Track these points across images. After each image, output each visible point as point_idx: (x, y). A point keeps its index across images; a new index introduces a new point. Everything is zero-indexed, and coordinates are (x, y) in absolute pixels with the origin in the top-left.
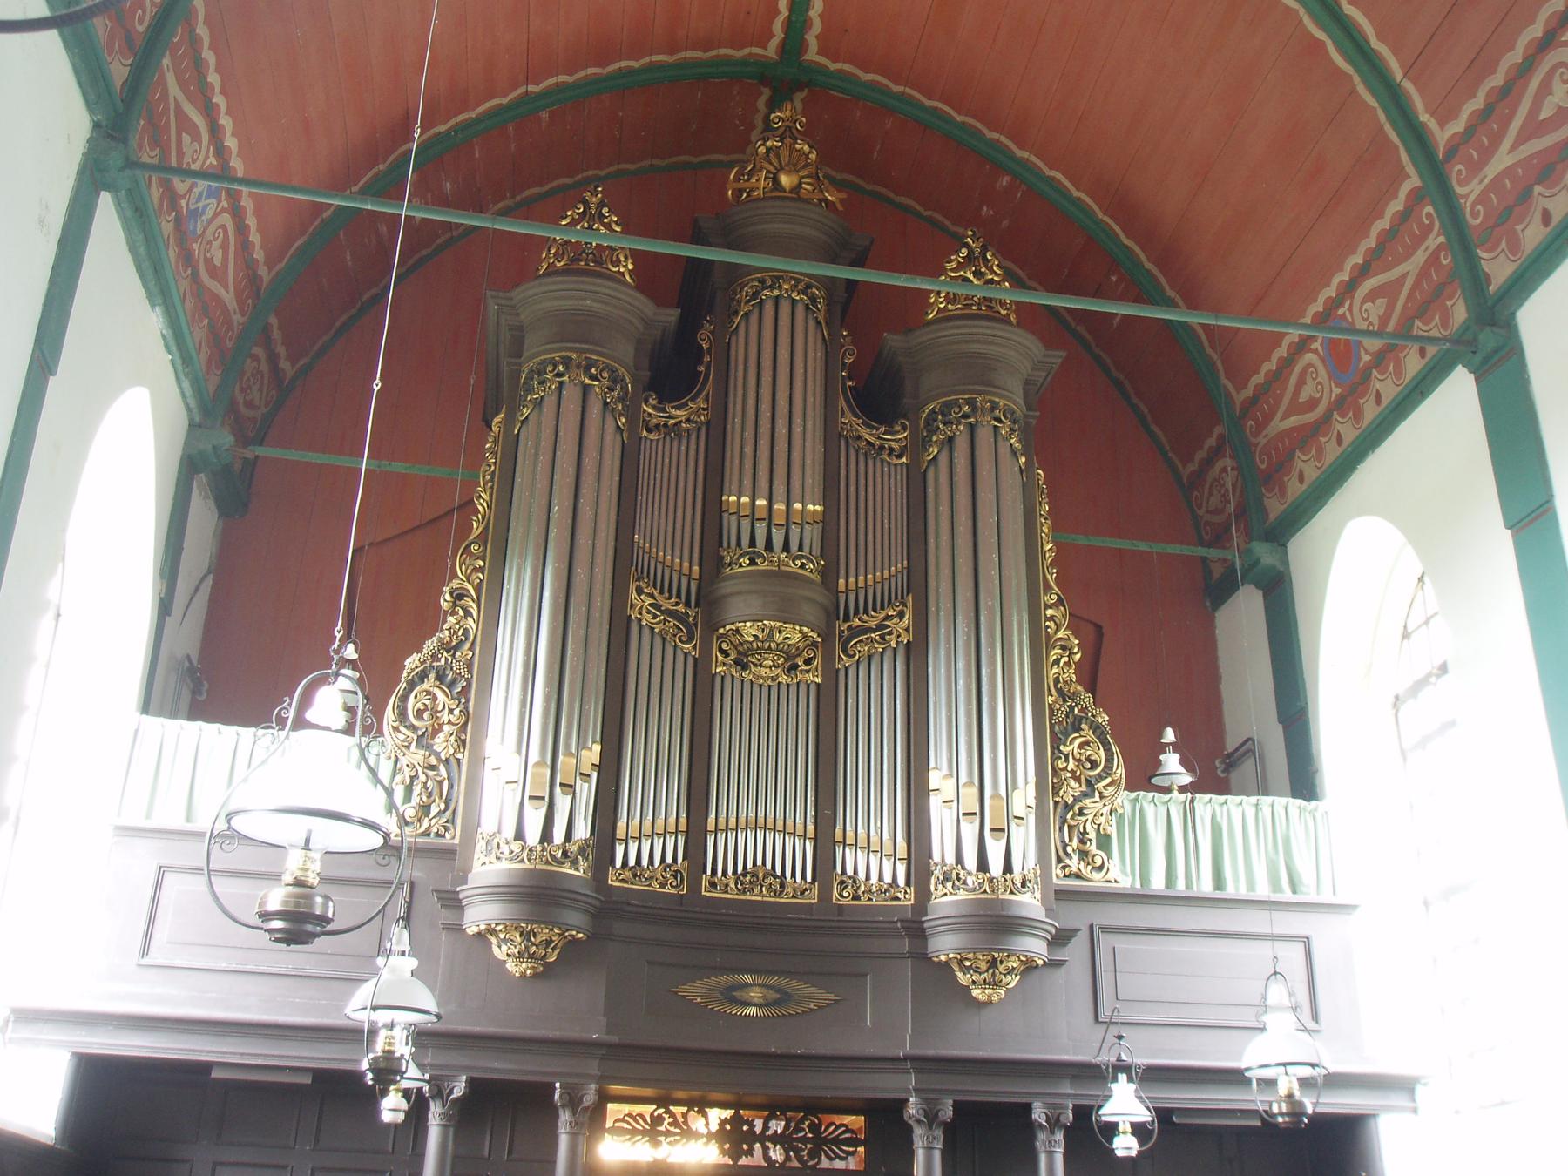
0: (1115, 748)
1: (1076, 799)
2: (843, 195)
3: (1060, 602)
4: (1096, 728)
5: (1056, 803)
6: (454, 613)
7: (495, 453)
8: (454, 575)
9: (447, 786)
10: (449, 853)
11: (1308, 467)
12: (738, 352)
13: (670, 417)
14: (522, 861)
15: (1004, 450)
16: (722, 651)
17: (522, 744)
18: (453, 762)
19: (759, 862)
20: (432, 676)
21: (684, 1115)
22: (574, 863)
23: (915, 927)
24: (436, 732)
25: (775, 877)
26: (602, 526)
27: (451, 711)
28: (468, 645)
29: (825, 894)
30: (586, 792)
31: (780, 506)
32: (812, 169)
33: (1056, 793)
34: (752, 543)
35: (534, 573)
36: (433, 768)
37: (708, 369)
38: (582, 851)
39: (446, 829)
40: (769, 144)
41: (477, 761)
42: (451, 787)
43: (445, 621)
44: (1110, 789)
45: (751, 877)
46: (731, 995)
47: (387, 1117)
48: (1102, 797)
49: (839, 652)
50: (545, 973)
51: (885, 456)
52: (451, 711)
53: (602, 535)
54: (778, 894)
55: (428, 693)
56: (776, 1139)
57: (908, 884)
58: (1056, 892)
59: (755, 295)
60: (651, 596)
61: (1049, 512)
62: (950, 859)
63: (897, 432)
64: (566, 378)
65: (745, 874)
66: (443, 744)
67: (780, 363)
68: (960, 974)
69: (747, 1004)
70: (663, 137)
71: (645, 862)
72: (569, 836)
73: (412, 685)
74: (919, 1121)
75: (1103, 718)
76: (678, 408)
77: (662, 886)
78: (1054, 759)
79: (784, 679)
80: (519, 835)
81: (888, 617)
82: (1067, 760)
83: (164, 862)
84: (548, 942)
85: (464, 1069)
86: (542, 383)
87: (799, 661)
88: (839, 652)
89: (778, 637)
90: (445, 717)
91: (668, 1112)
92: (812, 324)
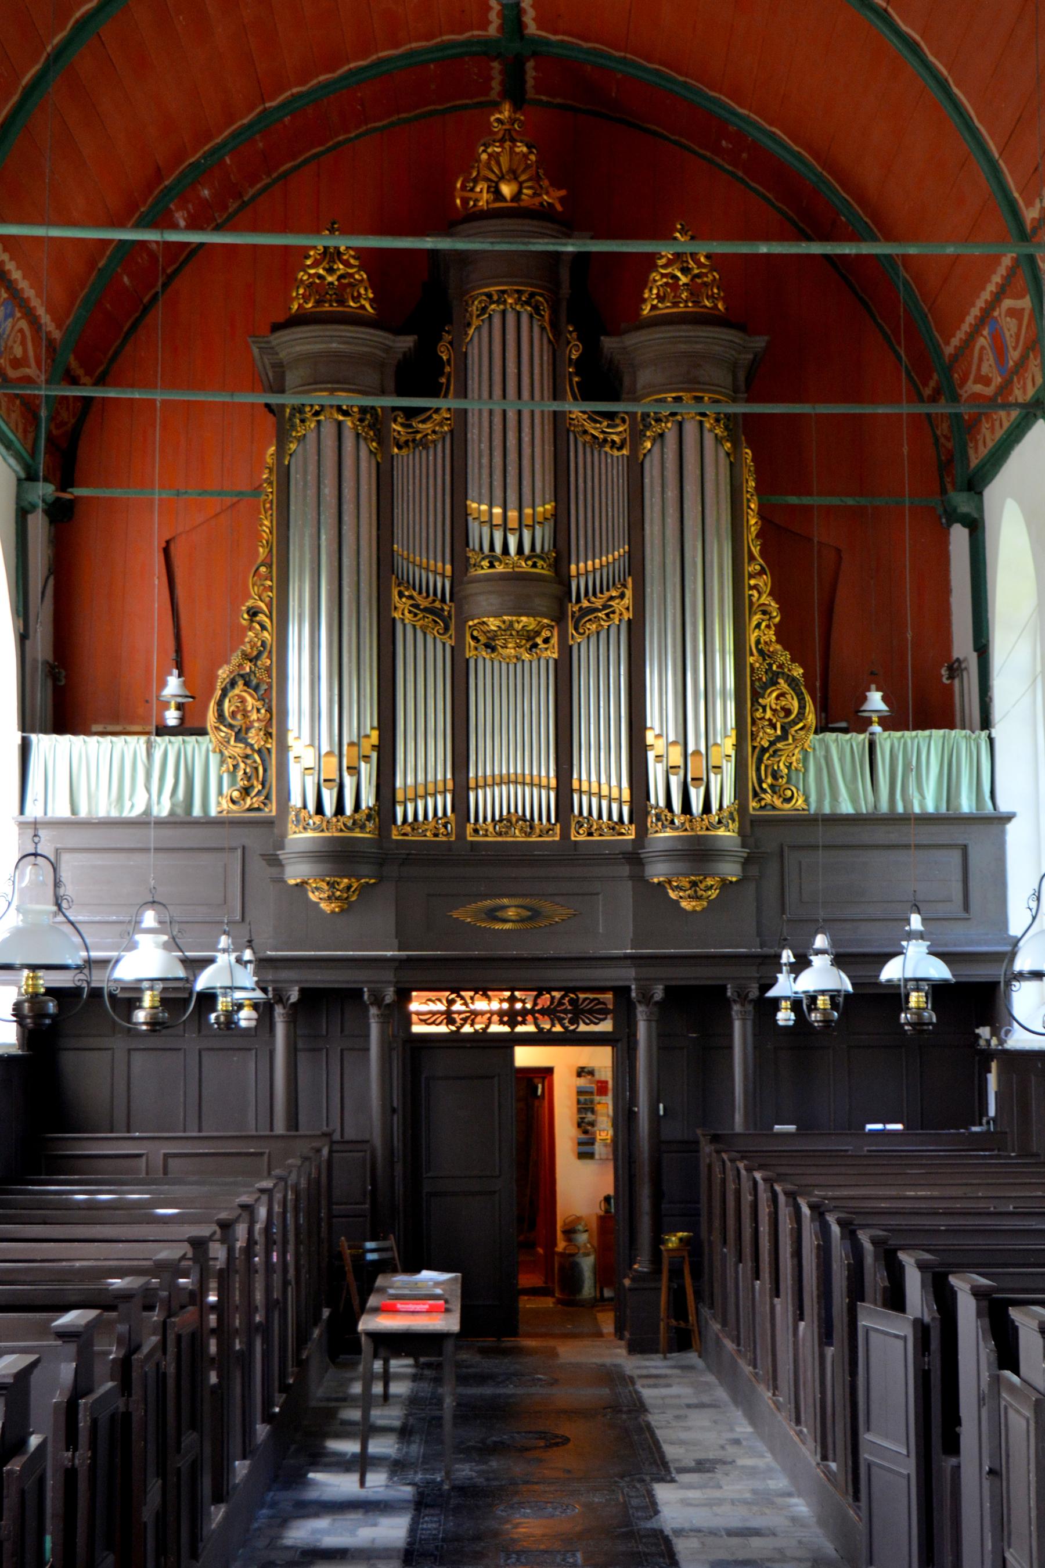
0: (808, 698)
1: (772, 743)
2: (562, 193)
3: (762, 572)
4: (792, 681)
5: (754, 748)
6: (251, 628)
7: (270, 483)
8: (249, 596)
9: (262, 768)
10: (269, 823)
11: (989, 436)
12: (473, 352)
13: (418, 432)
14: (322, 831)
15: (709, 439)
16: (474, 638)
17: (314, 741)
18: (265, 751)
19: (512, 810)
20: (241, 683)
21: (472, 998)
22: (363, 827)
23: (634, 857)
24: (248, 730)
25: (525, 821)
26: (364, 543)
27: (258, 710)
28: (266, 654)
29: (565, 834)
30: (367, 771)
31: (513, 514)
32: (532, 171)
33: (753, 739)
34: (492, 548)
35: (312, 582)
36: (247, 757)
37: (448, 381)
38: (369, 817)
39: (265, 804)
40: (490, 150)
41: (283, 748)
42: (265, 770)
43: (246, 636)
44: (802, 733)
45: (506, 822)
46: (492, 914)
47: (243, 1024)
48: (794, 740)
49: (571, 630)
50: (348, 907)
51: (607, 449)
52: (258, 710)
53: (364, 554)
54: (529, 835)
55: (239, 696)
56: (543, 1012)
57: (631, 822)
58: (752, 821)
59: (484, 310)
60: (411, 597)
61: (756, 488)
62: (662, 803)
63: (617, 426)
64: (322, 418)
65: (501, 820)
66: (254, 737)
67: (503, 347)
68: (670, 891)
69: (505, 921)
70: (395, 137)
71: (421, 818)
72: (357, 807)
73: (224, 693)
74: (639, 1002)
75: (798, 672)
76: (423, 422)
77: (436, 835)
78: (754, 710)
79: (526, 656)
80: (320, 810)
81: (612, 598)
82: (764, 711)
83: (59, 846)
84: (349, 887)
85: (297, 982)
86: (303, 421)
87: (539, 640)
88: (571, 630)
89: (518, 627)
90: (254, 716)
91: (459, 996)
92: (536, 330)
